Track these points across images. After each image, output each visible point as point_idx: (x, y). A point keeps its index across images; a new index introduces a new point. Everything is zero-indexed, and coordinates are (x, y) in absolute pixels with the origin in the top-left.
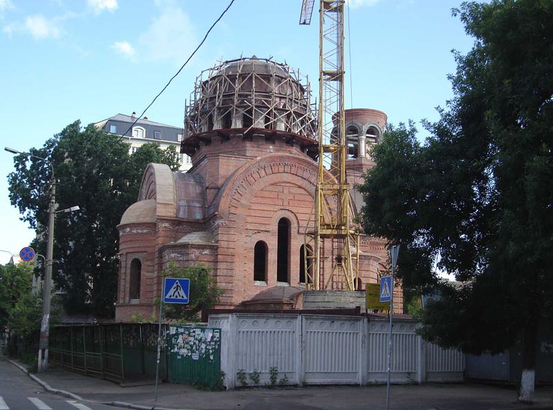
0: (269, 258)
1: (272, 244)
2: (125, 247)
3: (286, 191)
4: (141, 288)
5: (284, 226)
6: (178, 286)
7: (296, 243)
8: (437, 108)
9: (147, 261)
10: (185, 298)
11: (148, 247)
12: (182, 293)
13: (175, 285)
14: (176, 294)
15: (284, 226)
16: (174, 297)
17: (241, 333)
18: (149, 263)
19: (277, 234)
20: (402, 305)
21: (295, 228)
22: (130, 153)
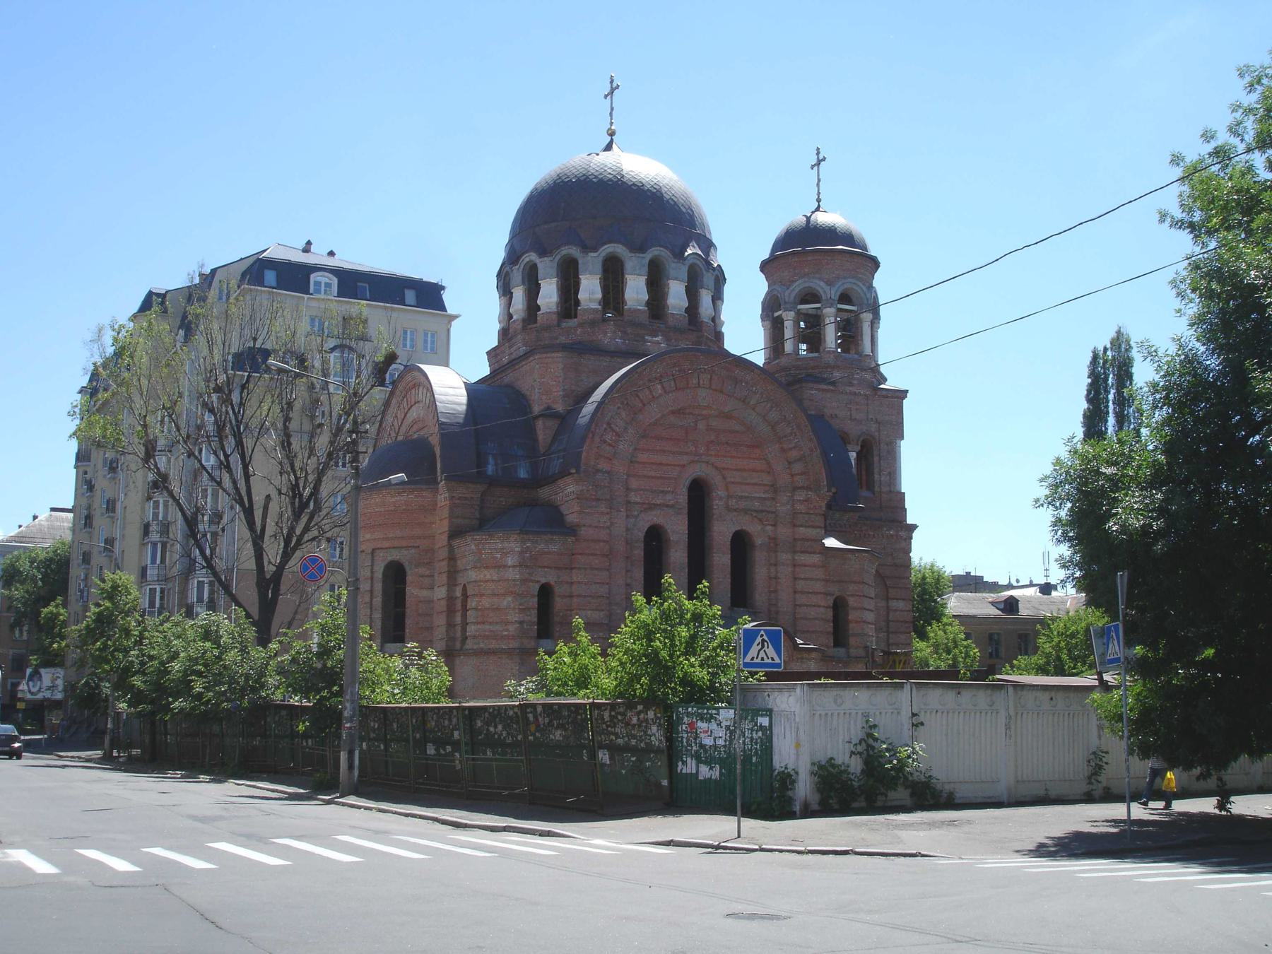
0: (672, 559)
1: (677, 529)
2: (368, 536)
3: (701, 426)
4: (408, 622)
5: (698, 493)
6: (763, 641)
7: (721, 531)
8: (309, 243)
9: (416, 566)
10: (777, 660)
11: (419, 538)
12: (771, 651)
13: (759, 639)
14: (762, 654)
15: (698, 493)
16: (759, 661)
17: (817, 716)
18: (421, 570)
19: (686, 511)
20: (536, 600)
21: (721, 499)
22: (1213, 362)
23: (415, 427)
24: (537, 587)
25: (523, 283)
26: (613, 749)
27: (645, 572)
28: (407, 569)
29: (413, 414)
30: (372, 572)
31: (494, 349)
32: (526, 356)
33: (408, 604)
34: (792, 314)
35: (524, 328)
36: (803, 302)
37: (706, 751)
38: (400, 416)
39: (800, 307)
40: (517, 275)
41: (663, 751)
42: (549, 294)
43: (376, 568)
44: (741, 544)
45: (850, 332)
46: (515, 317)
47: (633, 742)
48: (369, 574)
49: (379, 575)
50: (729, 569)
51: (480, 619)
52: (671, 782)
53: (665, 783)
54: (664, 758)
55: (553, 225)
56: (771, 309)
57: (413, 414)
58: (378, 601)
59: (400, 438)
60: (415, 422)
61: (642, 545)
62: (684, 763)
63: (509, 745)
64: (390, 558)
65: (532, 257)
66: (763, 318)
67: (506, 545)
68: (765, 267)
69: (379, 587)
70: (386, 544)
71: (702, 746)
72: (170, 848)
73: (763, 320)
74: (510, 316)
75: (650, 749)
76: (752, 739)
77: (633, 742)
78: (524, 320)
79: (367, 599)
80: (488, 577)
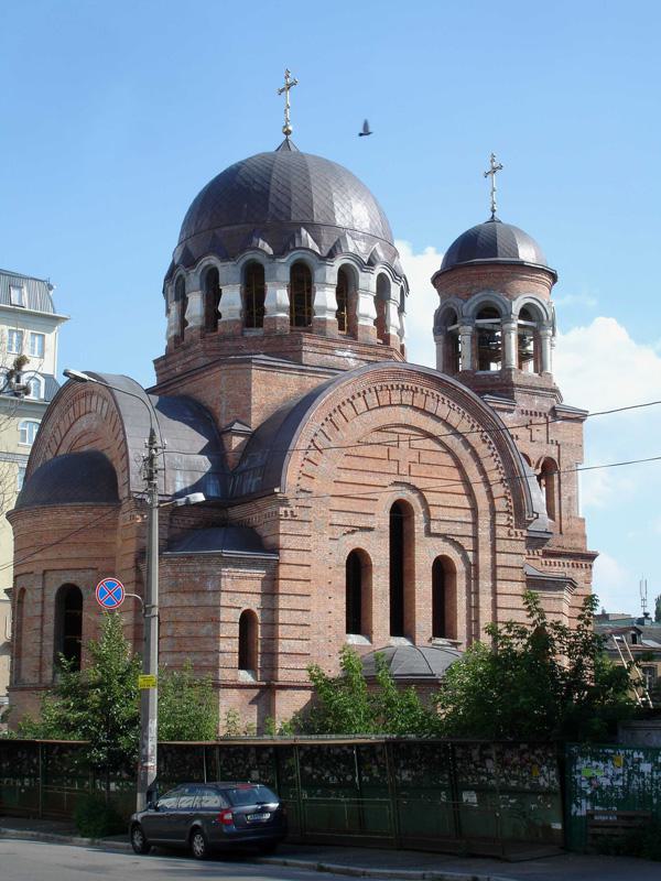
1: (379, 554)
7: (424, 554)
23: (83, 441)
24: (238, 614)
25: (201, 288)
26: (481, 790)
27: (347, 600)
28: (84, 592)
29: (83, 424)
30: (43, 595)
31: (163, 358)
32: (207, 367)
33: (84, 631)
34: (470, 328)
35: (203, 337)
36: (480, 316)
37: (602, 792)
38: (64, 426)
39: (478, 321)
40: (194, 279)
41: (555, 794)
42: (232, 300)
43: (47, 591)
44: (442, 569)
45: (246, 291)
46: (191, 324)
47: (513, 783)
48: (40, 598)
49: (51, 598)
50: (389, 592)
51: (176, 649)
52: (564, 826)
53: (558, 826)
54: (557, 801)
55: (236, 227)
56: (446, 323)
57: (83, 424)
58: (50, 627)
59: (63, 451)
60: (85, 433)
61: (344, 569)
62: (579, 805)
63: (333, 786)
64: (64, 581)
65: (213, 260)
66: (436, 332)
67: (206, 568)
68: (437, 280)
69: (51, 612)
70: (60, 565)
71: (599, 788)
72: (378, 868)
73: (435, 333)
74: (184, 323)
75: (536, 791)
76: (652, 779)
77: (513, 783)
78: (202, 328)
79: (37, 624)
80: (186, 603)
